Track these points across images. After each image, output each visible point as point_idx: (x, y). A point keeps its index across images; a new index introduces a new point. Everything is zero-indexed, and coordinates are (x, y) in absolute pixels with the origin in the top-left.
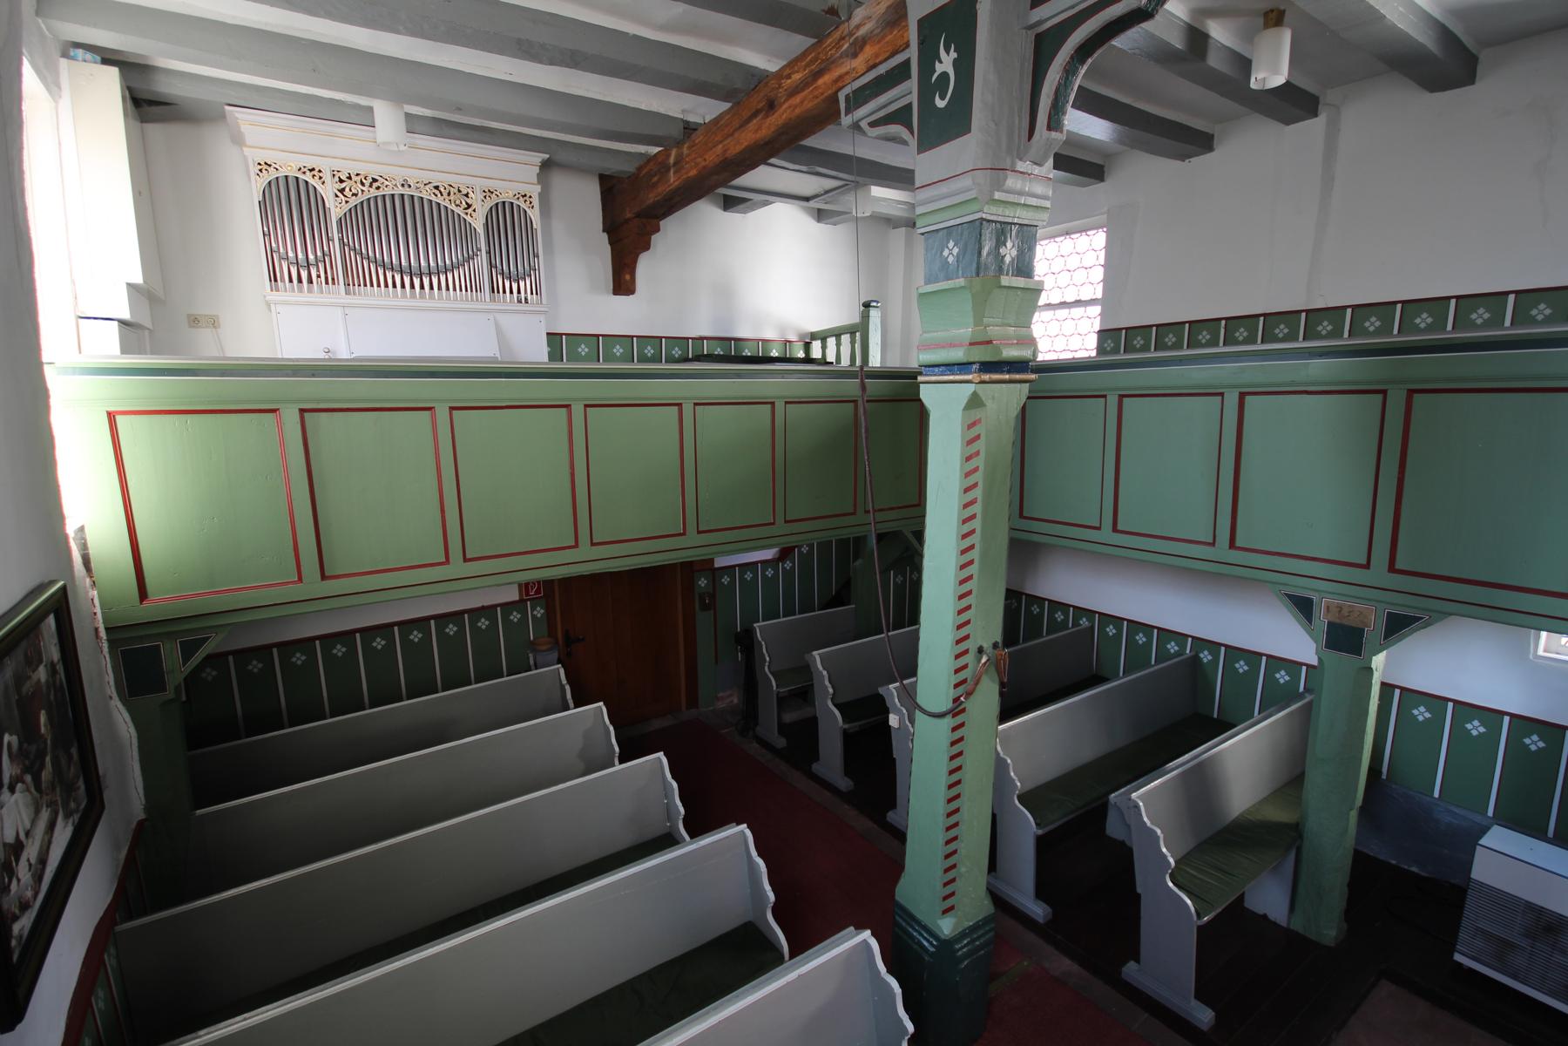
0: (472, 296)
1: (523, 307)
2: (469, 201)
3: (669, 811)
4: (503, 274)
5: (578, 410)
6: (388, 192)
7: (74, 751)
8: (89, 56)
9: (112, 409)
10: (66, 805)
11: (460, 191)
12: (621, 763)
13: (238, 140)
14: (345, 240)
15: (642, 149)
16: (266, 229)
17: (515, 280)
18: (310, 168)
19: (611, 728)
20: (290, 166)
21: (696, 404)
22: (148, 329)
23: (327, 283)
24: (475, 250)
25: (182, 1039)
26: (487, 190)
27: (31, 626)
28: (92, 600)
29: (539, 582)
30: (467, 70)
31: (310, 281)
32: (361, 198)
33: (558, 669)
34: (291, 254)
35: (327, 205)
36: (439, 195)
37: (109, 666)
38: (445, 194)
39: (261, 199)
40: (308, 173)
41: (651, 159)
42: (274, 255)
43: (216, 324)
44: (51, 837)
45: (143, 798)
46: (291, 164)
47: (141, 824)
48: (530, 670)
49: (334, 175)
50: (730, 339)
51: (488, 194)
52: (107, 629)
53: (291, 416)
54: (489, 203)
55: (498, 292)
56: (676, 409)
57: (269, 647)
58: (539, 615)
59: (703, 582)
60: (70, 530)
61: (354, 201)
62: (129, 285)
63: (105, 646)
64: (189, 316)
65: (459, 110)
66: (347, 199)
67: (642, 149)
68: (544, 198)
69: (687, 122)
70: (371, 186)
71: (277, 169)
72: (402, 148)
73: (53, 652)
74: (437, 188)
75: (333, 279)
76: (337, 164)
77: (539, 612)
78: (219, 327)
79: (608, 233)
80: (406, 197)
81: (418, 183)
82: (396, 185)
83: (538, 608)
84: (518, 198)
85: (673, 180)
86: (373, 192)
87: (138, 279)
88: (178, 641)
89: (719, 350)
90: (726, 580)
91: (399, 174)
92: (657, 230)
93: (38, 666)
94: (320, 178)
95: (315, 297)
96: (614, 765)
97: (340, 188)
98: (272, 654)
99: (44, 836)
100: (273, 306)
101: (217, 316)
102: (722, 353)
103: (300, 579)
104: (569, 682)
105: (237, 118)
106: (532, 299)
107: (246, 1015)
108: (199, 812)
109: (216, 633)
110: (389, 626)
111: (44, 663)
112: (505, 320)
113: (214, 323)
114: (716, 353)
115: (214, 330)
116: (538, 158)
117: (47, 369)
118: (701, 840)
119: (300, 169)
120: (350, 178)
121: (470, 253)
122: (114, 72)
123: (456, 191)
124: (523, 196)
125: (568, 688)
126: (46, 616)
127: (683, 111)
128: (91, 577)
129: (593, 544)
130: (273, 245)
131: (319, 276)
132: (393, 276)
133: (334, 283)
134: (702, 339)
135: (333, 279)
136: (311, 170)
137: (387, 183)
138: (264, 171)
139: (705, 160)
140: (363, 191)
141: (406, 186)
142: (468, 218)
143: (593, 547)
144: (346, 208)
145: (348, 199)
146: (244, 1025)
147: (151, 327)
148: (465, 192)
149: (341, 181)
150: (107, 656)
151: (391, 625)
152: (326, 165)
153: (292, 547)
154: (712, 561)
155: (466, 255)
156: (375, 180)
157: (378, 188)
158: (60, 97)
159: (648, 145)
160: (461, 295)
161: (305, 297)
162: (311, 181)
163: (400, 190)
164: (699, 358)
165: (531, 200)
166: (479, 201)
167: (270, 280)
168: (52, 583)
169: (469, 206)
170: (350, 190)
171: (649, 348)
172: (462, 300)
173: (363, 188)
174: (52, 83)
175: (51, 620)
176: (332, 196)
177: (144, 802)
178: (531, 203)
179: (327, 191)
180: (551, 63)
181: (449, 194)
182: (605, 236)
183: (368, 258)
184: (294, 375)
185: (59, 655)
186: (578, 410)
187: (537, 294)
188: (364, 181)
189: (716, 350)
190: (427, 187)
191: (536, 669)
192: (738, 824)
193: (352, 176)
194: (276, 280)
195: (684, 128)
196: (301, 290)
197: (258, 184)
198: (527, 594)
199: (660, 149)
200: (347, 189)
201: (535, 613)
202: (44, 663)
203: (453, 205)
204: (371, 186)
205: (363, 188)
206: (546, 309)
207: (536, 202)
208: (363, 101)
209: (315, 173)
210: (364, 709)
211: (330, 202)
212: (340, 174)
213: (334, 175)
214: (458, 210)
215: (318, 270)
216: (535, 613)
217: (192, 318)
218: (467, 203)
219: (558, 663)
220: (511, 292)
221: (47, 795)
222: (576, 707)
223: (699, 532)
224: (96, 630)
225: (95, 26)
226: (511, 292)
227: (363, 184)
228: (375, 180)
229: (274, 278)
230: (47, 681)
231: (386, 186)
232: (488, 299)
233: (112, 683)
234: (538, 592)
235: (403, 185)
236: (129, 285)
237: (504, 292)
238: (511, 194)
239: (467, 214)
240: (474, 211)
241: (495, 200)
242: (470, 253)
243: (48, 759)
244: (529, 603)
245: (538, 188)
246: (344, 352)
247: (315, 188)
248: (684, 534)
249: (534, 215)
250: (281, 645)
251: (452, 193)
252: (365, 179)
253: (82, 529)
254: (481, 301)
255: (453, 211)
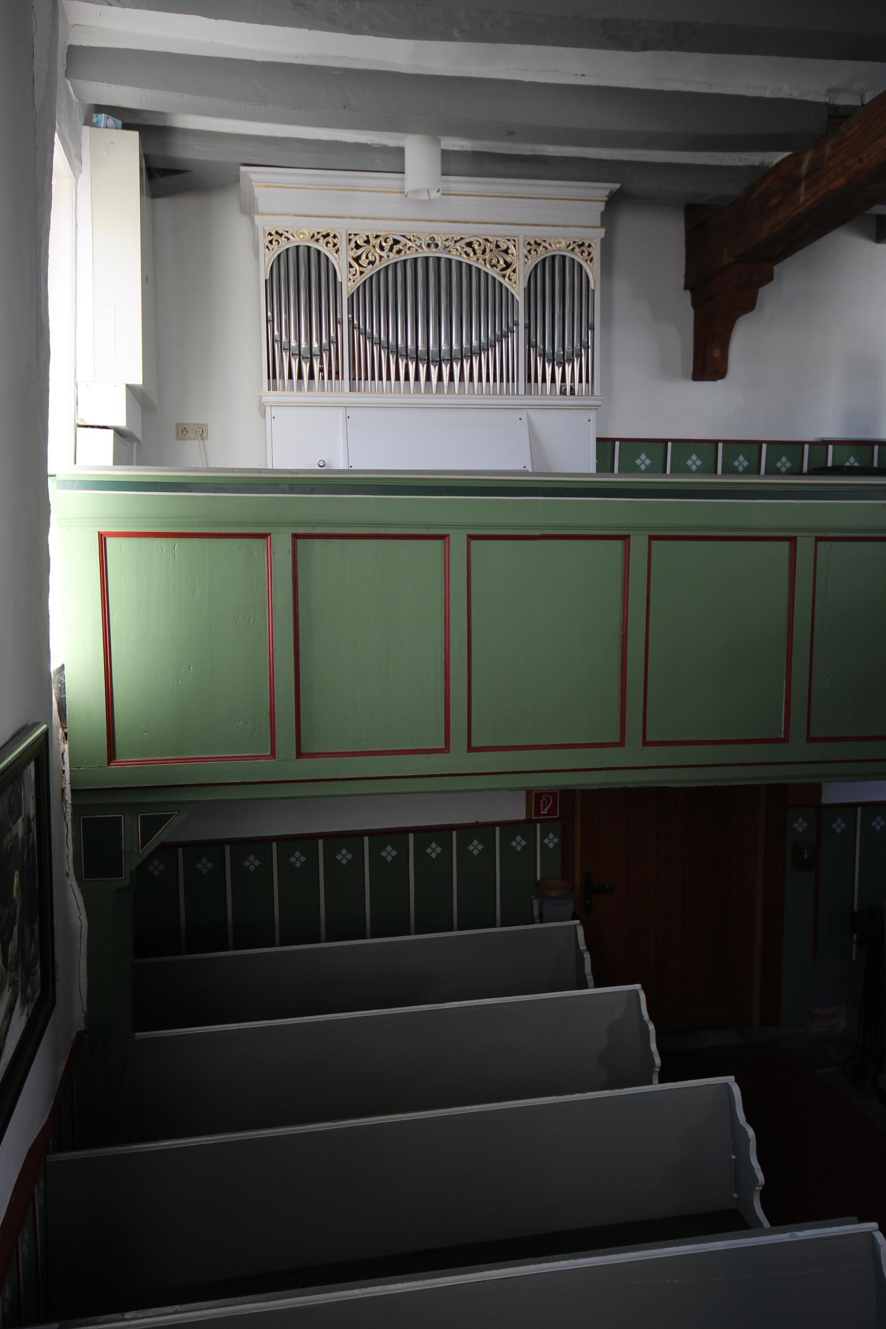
0: (501, 387)
1: (568, 400)
2: (509, 259)
3: (740, 1168)
4: (544, 355)
5: (639, 542)
6: (410, 255)
7: (36, 926)
8: (111, 121)
9: (102, 530)
10: (24, 991)
11: (498, 246)
12: (661, 1081)
13: (249, 209)
14: (356, 322)
15: (755, 158)
16: (269, 314)
17: (559, 364)
18: (325, 233)
19: (651, 1027)
20: (303, 234)
21: (818, 539)
22: (139, 441)
23: (330, 378)
24: (510, 325)
25: (107, 1317)
26: (532, 242)
27: (16, 770)
28: (63, 754)
29: (554, 794)
30: (526, 79)
31: (311, 376)
32: (379, 266)
33: (575, 926)
34: (293, 344)
35: (339, 279)
36: (472, 254)
37: (70, 835)
38: (479, 252)
39: (268, 277)
40: (321, 240)
41: (765, 173)
42: (276, 345)
43: (204, 435)
44: (10, 1022)
45: (85, 1004)
46: (302, 231)
47: (80, 1034)
48: (533, 923)
49: (350, 240)
50: (870, 444)
51: (534, 247)
52: (73, 791)
53: (282, 542)
54: (534, 259)
55: (536, 381)
56: (786, 545)
57: (221, 843)
58: (551, 845)
59: (800, 825)
60: (54, 666)
61: (370, 271)
62: (127, 386)
63: (69, 810)
64: (178, 425)
65: (510, 134)
66: (362, 269)
67: (755, 158)
68: (607, 245)
69: (836, 108)
70: (391, 250)
71: (288, 239)
72: (435, 195)
73: (30, 807)
74: (469, 244)
75: (337, 373)
76: (356, 226)
77: (552, 841)
78: (207, 439)
79: (691, 291)
80: (431, 260)
81: (447, 240)
82: (420, 246)
83: (551, 836)
84: (573, 249)
85: (804, 197)
86: (394, 258)
87: (137, 380)
88: (139, 815)
89: (852, 460)
90: (839, 826)
91: (425, 230)
92: (769, 278)
93: (17, 819)
94: (335, 245)
95: (315, 397)
96: (651, 1083)
97: (355, 256)
98: (224, 849)
99: (3, 1020)
100: (268, 409)
101: (206, 425)
102: (856, 464)
103: (273, 754)
104: (589, 949)
105: (252, 180)
106: (581, 388)
107: (177, 1307)
108: (139, 1035)
109: (179, 812)
110: (359, 835)
111: (22, 817)
112: (544, 421)
113: (202, 433)
114: (848, 464)
115: (201, 441)
116: (603, 190)
117: (50, 481)
118: (800, 1230)
119: (313, 236)
120: (367, 242)
121: (504, 328)
122: (134, 136)
123: (493, 246)
124: (580, 246)
125: (587, 956)
126: (27, 763)
127: (830, 91)
128: (63, 728)
129: (645, 743)
130: (276, 333)
131: (321, 370)
132: (407, 366)
133: (337, 378)
134: (825, 443)
135: (337, 373)
136: (325, 237)
137: (410, 244)
138: (274, 242)
139: (861, 160)
140: (381, 257)
141: (433, 246)
142: (506, 283)
143: (646, 748)
144: (360, 280)
145: (362, 269)
146: (153, 1323)
147: (141, 439)
148: (503, 246)
149: (358, 247)
150: (70, 824)
151: (361, 834)
152: (340, 228)
153: (268, 710)
154: (817, 789)
155: (498, 332)
156: (396, 242)
157: (399, 252)
158: (81, 171)
159: (763, 150)
160: (488, 387)
161: (305, 396)
162: (324, 250)
163: (426, 252)
164: (838, 470)
165: (590, 250)
166: (522, 257)
167: (269, 378)
168: (36, 725)
169: (508, 265)
170: (367, 257)
171: (741, 458)
172: (495, 393)
173: (382, 254)
174: (75, 159)
175: (32, 767)
176: (345, 266)
177: (85, 1009)
178: (589, 254)
179: (340, 261)
180: (645, 47)
181: (484, 252)
182: (688, 295)
183: (380, 344)
184: (291, 491)
185: (34, 811)
186: (639, 542)
187: (587, 381)
188: (384, 244)
189: (848, 460)
190: (458, 244)
191: (542, 922)
192: (862, 1220)
193: (371, 239)
194: (274, 377)
195: (830, 117)
196: (300, 389)
197: (267, 258)
198: (538, 813)
199: (786, 154)
200: (364, 257)
201: (546, 841)
202: (22, 817)
203: (488, 265)
204: (391, 250)
205: (382, 254)
206: (598, 403)
207: (596, 253)
208: (389, 139)
209: (330, 239)
210: (319, 942)
211: (343, 275)
212: (357, 237)
213: (350, 240)
214: (493, 273)
215: (321, 363)
216: (546, 841)
217: (181, 428)
218: (505, 262)
219: (574, 917)
220: (553, 380)
221: (11, 972)
222: (597, 985)
223: (810, 740)
224: (63, 790)
225: (122, 82)
226: (553, 380)
227: (382, 248)
228: (396, 242)
229: (272, 375)
230: (23, 838)
231: (409, 249)
232: (522, 391)
233: (71, 857)
234: (552, 811)
235: (429, 245)
236: (127, 386)
237: (544, 380)
238: (564, 244)
239: (504, 276)
240: (514, 271)
241: (542, 254)
242: (504, 328)
243: (16, 929)
244: (538, 825)
245: (601, 233)
246: (339, 463)
247: (327, 258)
248: (785, 740)
249: (593, 271)
250: (235, 843)
251: (488, 250)
252: (386, 242)
253: (62, 667)
254: (513, 394)
255: (487, 274)
